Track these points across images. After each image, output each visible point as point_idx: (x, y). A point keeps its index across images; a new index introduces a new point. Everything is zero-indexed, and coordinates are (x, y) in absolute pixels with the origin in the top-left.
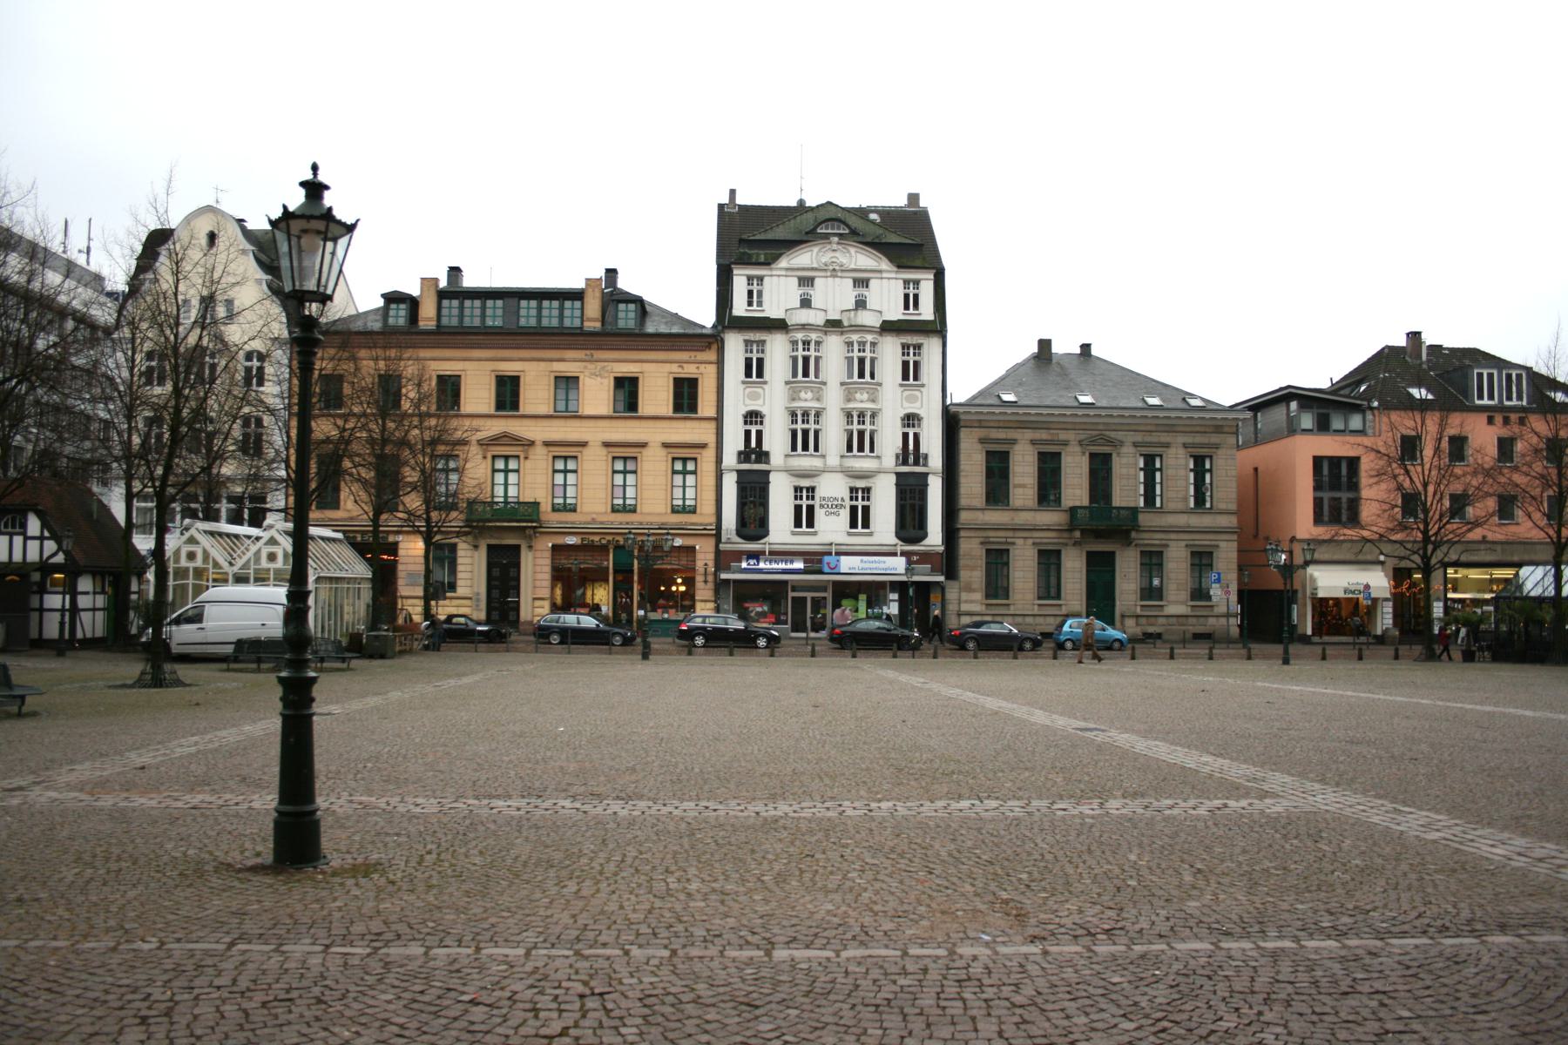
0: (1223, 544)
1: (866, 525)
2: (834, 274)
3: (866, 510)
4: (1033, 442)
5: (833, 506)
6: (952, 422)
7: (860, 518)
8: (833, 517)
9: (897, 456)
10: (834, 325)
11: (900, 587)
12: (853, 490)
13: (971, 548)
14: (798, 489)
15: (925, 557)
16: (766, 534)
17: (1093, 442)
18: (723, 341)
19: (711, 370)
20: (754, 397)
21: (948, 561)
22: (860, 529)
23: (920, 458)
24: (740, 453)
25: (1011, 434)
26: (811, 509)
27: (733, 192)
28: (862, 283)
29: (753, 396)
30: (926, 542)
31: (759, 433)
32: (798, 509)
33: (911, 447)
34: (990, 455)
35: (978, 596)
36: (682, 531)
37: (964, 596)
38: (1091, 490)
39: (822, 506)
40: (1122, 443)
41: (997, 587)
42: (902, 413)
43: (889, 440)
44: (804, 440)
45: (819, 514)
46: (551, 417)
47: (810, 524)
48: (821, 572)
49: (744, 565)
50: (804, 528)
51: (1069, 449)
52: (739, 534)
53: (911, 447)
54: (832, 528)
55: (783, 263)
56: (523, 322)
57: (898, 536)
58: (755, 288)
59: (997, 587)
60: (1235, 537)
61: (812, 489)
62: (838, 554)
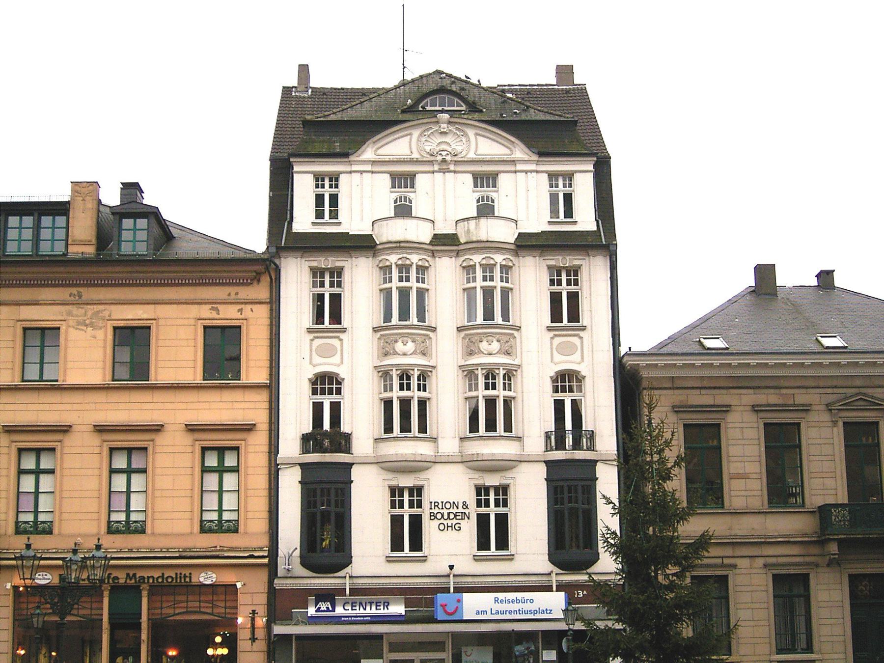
0: (743, 563)
1: (503, 542)
4: (756, 409)
5: (451, 516)
7: (493, 533)
8: (451, 533)
9: (547, 436)
10: (445, 243)
12: (481, 491)
14: (395, 492)
16: (348, 561)
17: (848, 405)
18: (278, 271)
19: (261, 313)
23: (582, 436)
24: (305, 438)
25: (723, 398)
26: (416, 522)
28: (485, 179)
31: (336, 408)
32: (396, 522)
33: (569, 425)
39: (433, 516)
42: (552, 370)
43: (535, 414)
44: (405, 414)
45: (429, 528)
47: (417, 544)
48: (432, 620)
49: (311, 611)
52: (304, 563)
53: (569, 425)
54: (449, 549)
55: (368, 153)
57: (552, 559)
61: (417, 491)
62: (459, 590)
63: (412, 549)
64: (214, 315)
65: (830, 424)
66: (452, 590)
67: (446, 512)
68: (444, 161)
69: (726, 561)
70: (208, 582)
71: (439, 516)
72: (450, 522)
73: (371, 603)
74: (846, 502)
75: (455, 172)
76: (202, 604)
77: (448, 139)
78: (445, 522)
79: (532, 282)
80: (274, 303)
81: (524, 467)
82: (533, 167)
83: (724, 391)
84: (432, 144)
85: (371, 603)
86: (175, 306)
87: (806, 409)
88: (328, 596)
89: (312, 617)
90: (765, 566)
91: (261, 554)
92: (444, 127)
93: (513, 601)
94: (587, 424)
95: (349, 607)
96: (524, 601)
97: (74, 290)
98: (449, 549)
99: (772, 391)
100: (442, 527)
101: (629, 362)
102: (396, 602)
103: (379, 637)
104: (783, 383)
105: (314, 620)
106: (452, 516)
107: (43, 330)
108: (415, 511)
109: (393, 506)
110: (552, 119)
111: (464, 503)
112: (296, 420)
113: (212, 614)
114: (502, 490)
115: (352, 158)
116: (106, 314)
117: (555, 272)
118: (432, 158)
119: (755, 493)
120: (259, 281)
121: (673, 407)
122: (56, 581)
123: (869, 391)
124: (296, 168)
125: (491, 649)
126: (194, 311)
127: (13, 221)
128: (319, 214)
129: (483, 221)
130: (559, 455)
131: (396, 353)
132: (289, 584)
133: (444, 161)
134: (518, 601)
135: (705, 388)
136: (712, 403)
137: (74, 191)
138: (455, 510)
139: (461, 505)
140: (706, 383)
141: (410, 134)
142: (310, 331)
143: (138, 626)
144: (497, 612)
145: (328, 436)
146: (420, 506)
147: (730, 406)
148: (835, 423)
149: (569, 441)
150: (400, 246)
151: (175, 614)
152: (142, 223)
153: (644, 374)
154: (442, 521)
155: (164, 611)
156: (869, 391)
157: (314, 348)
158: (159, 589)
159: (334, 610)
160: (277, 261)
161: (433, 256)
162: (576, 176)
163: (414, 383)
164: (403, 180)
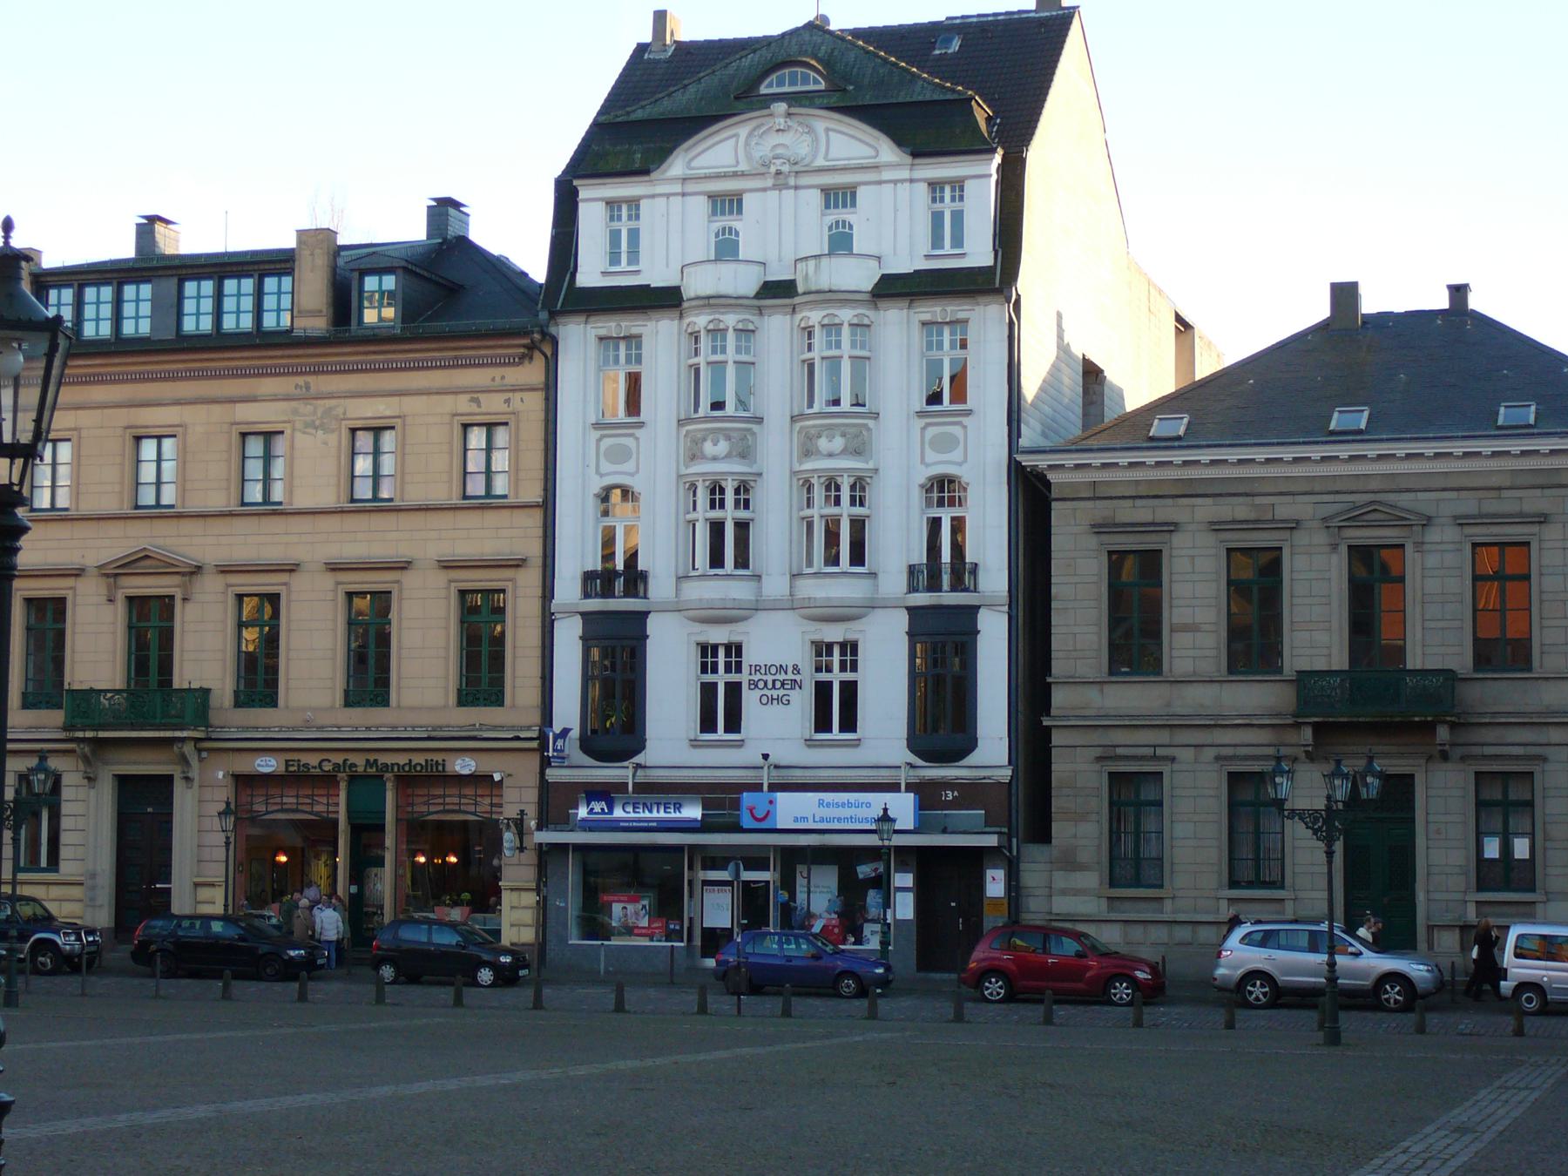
0: (1186, 755)
1: (849, 723)
2: (781, 182)
3: (850, 690)
4: (1216, 527)
5: (780, 683)
6: (1032, 496)
7: (836, 708)
8: (776, 708)
9: (912, 570)
10: (778, 291)
11: (926, 862)
12: (822, 649)
13: (1076, 770)
14: (707, 650)
15: (971, 793)
16: (640, 747)
17: (1355, 518)
18: (555, 342)
19: (533, 404)
20: (945, 444)
21: (1029, 802)
22: (836, 733)
23: (963, 575)
24: (588, 577)
25: (1166, 511)
26: (734, 690)
27: (660, 17)
28: (839, 197)
29: (616, 455)
30: (973, 759)
31: (958, 525)
32: (708, 691)
33: (946, 556)
34: (1116, 559)
35: (1091, 880)
36: (469, 741)
37: (1060, 880)
38: (1050, 635)
39: (754, 685)
40: (1428, 522)
41: (1133, 864)
42: (922, 475)
43: (897, 542)
44: (729, 546)
45: (750, 698)
46: (231, 514)
47: (733, 724)
48: (736, 828)
49: (582, 812)
50: (721, 734)
51: (1301, 538)
52: (587, 746)
53: (946, 556)
54: (777, 728)
55: (677, 165)
56: (189, 325)
57: (913, 745)
58: (947, 207)
59: (1133, 864)
60: (9, 736)
61: (734, 649)
62: (774, 788)
63: (842, 729)
64: (474, 408)
65: (1328, 549)
66: (765, 787)
67: (770, 678)
68: (778, 173)
69: (1159, 752)
70: (466, 772)
71: (761, 685)
72: (775, 693)
73: (658, 804)
74: (1346, 667)
75: (796, 188)
76: (301, 800)
78: (769, 693)
81: (879, 614)
82: (905, 174)
83: (1169, 501)
84: (768, 145)
85: (658, 804)
86: (424, 398)
87: (1294, 526)
89: (583, 820)
90: (1218, 758)
91: (528, 734)
93: (843, 805)
95: (630, 809)
96: (858, 805)
97: (300, 380)
99: (1241, 499)
100: (764, 700)
101: (1027, 461)
102: (692, 802)
104: (1257, 488)
105: (587, 825)
106: (778, 685)
108: (733, 677)
109: (704, 670)
110: (942, 97)
111: (796, 669)
113: (474, 814)
115: (654, 175)
116: (340, 411)
118: (763, 170)
119: (1207, 653)
120: (531, 358)
121: (1093, 526)
122: (282, 770)
123: (1391, 497)
124: (582, 194)
125: (836, 868)
126: (449, 403)
128: (614, 258)
129: (835, 261)
131: (704, 457)
133: (778, 173)
134: (850, 804)
135: (1141, 497)
136: (1149, 519)
137: (300, 241)
138: (782, 677)
139: (790, 670)
140: (1143, 491)
141: (736, 136)
143: (382, 828)
144: (822, 820)
146: (739, 670)
147: (1175, 524)
148: (1334, 547)
149: (946, 579)
150: (711, 302)
151: (268, 813)
154: (765, 692)
155: (416, 809)
156: (1391, 497)
157: (927, 438)
158: (408, 780)
159: (611, 812)
160: (553, 330)
161: (761, 314)
162: (643, 203)
163: (730, 497)
164: (726, 203)
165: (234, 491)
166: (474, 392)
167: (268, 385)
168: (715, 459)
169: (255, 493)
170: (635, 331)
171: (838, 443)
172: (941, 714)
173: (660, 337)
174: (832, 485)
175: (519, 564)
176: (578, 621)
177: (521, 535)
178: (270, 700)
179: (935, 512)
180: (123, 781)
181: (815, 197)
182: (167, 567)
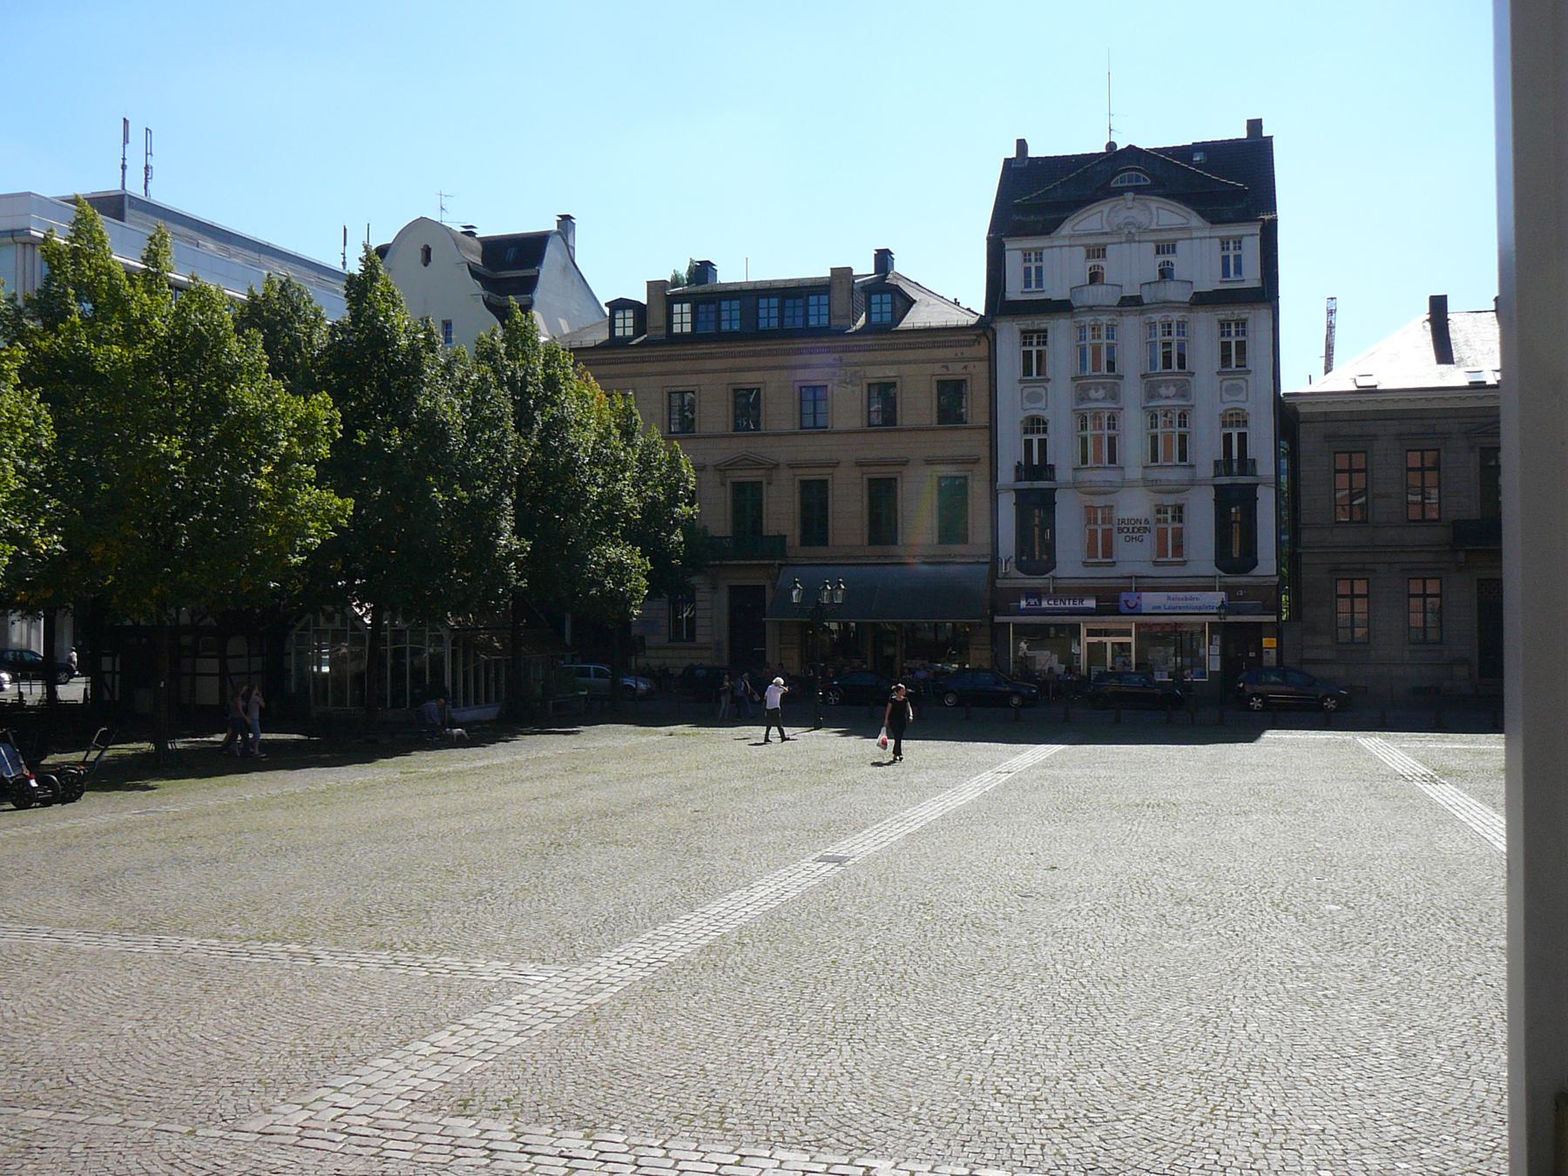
5: (1135, 530)
9: (1216, 463)
10: (1131, 303)
19: (981, 368)
20: (1034, 398)
23: (1247, 465)
26: (1108, 536)
33: (1235, 455)
39: (1121, 530)
42: (1022, 415)
43: (1207, 448)
45: (1119, 540)
52: (1020, 566)
53: (1235, 455)
55: (1066, 229)
77: (1134, 212)
79: (1204, 334)
80: (992, 360)
88: (1036, 594)
92: (1130, 204)
94: (1251, 453)
98: (1134, 557)
103: (1047, 626)
107: (815, 387)
112: (1010, 452)
114: (1179, 509)
117: (1225, 325)
127: (763, 302)
128: (1028, 284)
130: (1226, 480)
131: (1089, 399)
132: (1007, 583)
142: (1021, 381)
145: (1036, 469)
150: (1166, 305)
152: (887, 298)
153: (1302, 409)
165: (797, 421)
166: (944, 362)
167: (815, 359)
168: (1097, 400)
169: (809, 421)
170: (1043, 326)
171: (1172, 390)
172: (1235, 547)
173: (1061, 332)
174: (1097, 416)
175: (976, 461)
176: (1013, 495)
177: (974, 444)
178: (823, 540)
179: (1028, 437)
180: (733, 590)
181: (1083, 251)
182: (757, 464)
